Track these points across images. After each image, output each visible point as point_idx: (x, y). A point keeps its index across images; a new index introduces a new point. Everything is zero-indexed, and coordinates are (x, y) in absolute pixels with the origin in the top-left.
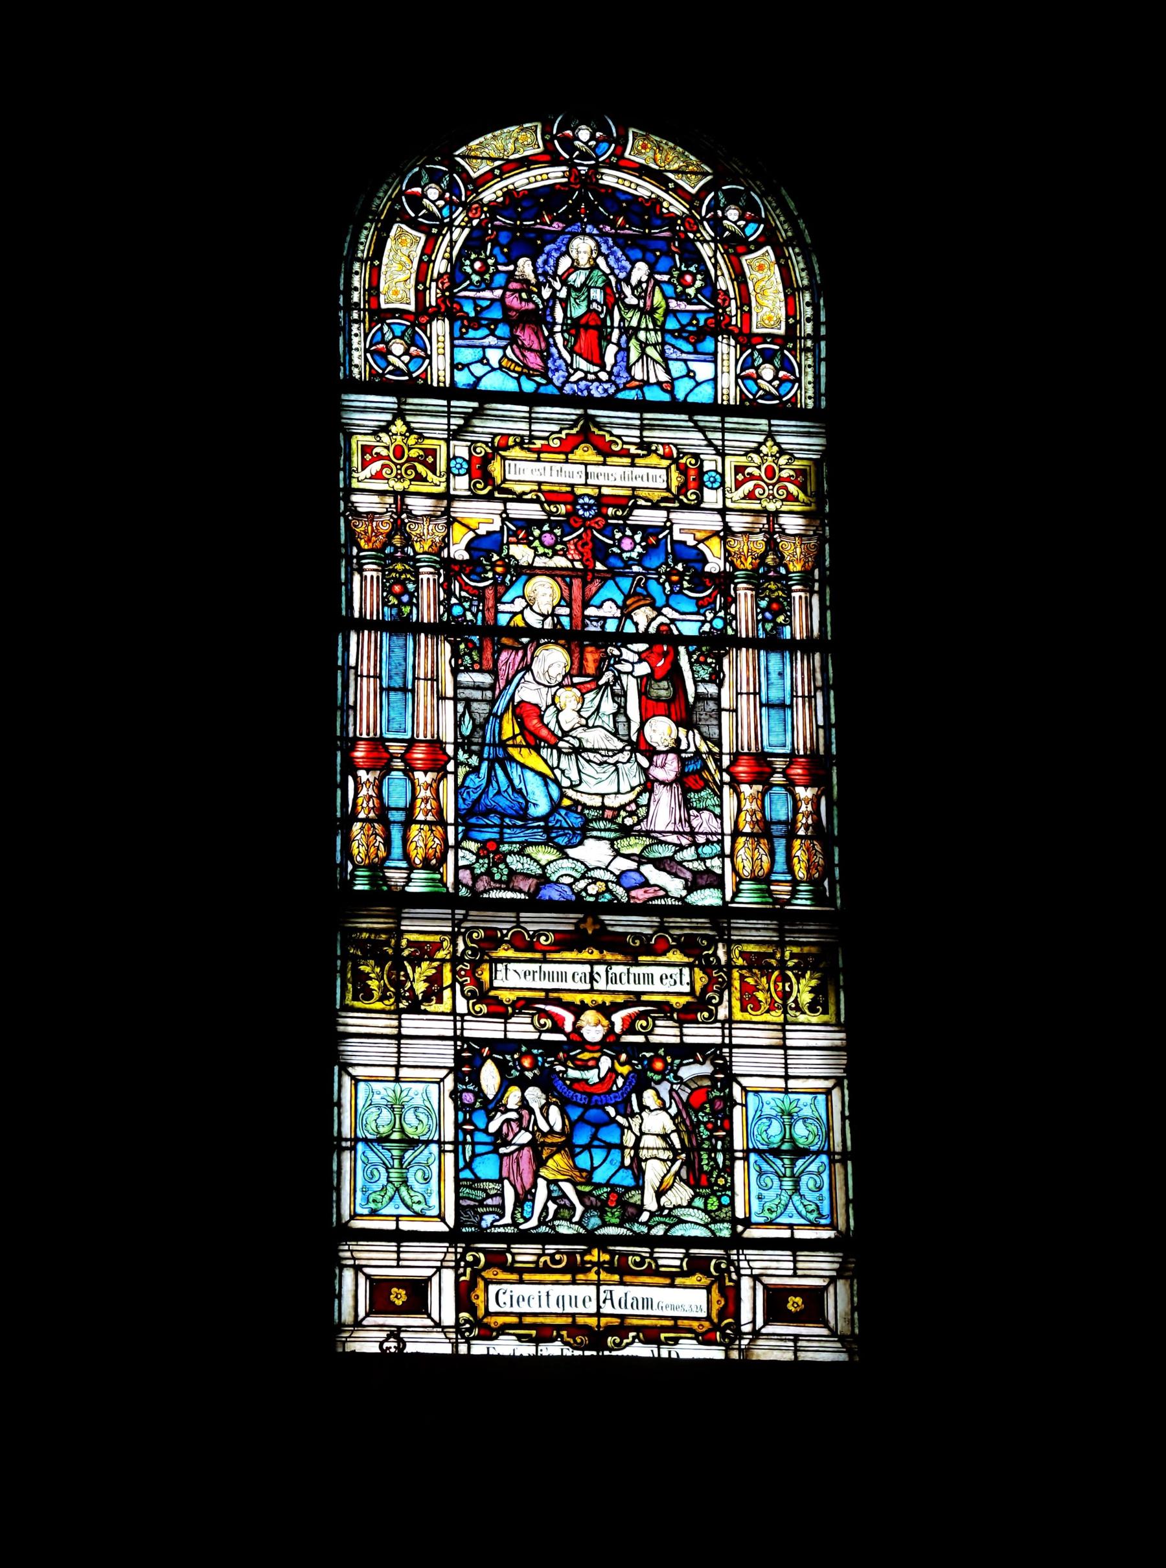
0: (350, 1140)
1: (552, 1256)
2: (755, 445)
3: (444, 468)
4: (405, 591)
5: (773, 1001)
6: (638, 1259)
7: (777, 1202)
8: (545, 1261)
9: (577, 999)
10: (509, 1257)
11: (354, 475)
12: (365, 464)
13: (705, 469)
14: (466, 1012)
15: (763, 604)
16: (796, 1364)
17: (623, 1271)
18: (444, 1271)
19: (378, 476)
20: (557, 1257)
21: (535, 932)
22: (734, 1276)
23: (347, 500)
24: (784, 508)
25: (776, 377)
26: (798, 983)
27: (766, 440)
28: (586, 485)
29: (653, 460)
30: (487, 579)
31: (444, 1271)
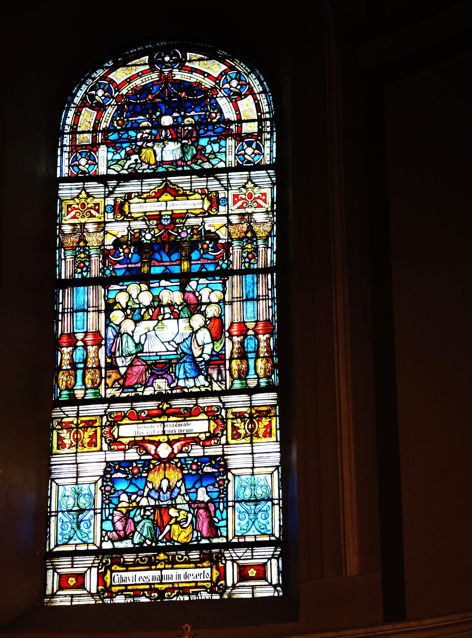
0: (55, 512)
1: (141, 558)
2: (244, 184)
3: (103, 211)
4: (85, 266)
5: (72, 443)
6: (180, 557)
7: (247, 525)
8: (138, 561)
9: (156, 439)
10: (122, 559)
11: (64, 218)
12: (68, 213)
13: (220, 197)
14: (107, 450)
15: (245, 255)
16: (254, 599)
17: (172, 563)
18: (93, 569)
19: (74, 217)
20: (143, 559)
21: (139, 411)
22: (224, 562)
23: (60, 229)
24: (89, 221)
25: (87, 163)
26: (84, 434)
27: (248, 182)
28: (166, 210)
29: (197, 196)
30: (121, 256)
31: (93, 569)
